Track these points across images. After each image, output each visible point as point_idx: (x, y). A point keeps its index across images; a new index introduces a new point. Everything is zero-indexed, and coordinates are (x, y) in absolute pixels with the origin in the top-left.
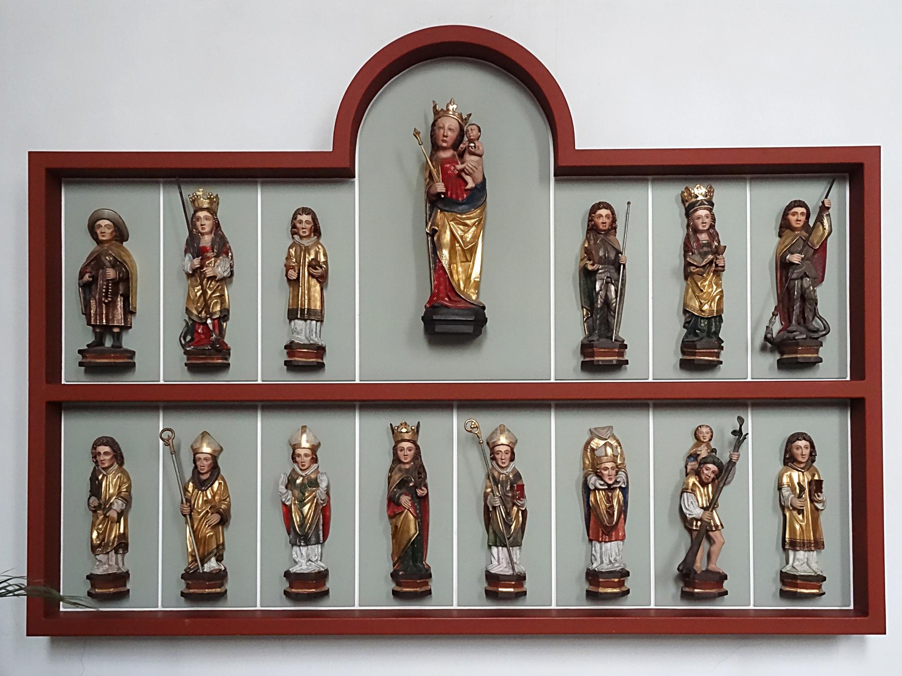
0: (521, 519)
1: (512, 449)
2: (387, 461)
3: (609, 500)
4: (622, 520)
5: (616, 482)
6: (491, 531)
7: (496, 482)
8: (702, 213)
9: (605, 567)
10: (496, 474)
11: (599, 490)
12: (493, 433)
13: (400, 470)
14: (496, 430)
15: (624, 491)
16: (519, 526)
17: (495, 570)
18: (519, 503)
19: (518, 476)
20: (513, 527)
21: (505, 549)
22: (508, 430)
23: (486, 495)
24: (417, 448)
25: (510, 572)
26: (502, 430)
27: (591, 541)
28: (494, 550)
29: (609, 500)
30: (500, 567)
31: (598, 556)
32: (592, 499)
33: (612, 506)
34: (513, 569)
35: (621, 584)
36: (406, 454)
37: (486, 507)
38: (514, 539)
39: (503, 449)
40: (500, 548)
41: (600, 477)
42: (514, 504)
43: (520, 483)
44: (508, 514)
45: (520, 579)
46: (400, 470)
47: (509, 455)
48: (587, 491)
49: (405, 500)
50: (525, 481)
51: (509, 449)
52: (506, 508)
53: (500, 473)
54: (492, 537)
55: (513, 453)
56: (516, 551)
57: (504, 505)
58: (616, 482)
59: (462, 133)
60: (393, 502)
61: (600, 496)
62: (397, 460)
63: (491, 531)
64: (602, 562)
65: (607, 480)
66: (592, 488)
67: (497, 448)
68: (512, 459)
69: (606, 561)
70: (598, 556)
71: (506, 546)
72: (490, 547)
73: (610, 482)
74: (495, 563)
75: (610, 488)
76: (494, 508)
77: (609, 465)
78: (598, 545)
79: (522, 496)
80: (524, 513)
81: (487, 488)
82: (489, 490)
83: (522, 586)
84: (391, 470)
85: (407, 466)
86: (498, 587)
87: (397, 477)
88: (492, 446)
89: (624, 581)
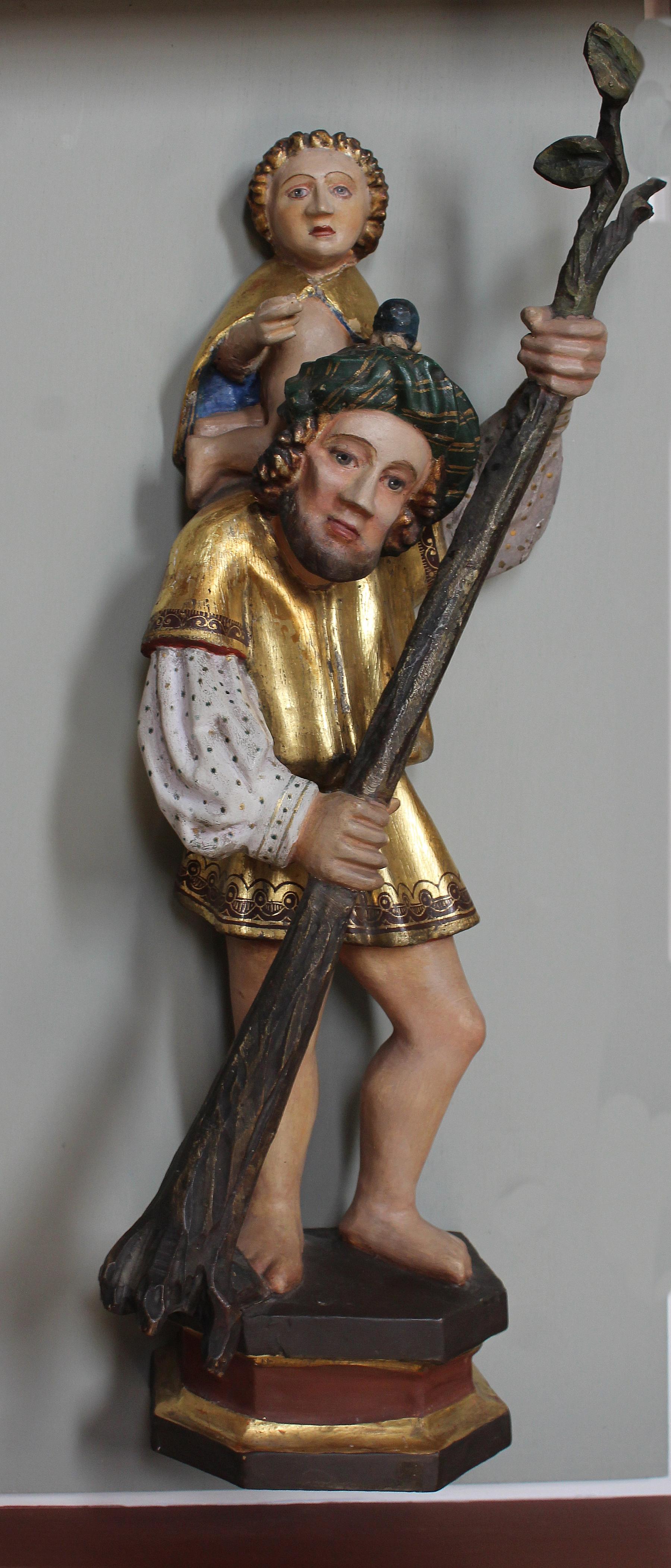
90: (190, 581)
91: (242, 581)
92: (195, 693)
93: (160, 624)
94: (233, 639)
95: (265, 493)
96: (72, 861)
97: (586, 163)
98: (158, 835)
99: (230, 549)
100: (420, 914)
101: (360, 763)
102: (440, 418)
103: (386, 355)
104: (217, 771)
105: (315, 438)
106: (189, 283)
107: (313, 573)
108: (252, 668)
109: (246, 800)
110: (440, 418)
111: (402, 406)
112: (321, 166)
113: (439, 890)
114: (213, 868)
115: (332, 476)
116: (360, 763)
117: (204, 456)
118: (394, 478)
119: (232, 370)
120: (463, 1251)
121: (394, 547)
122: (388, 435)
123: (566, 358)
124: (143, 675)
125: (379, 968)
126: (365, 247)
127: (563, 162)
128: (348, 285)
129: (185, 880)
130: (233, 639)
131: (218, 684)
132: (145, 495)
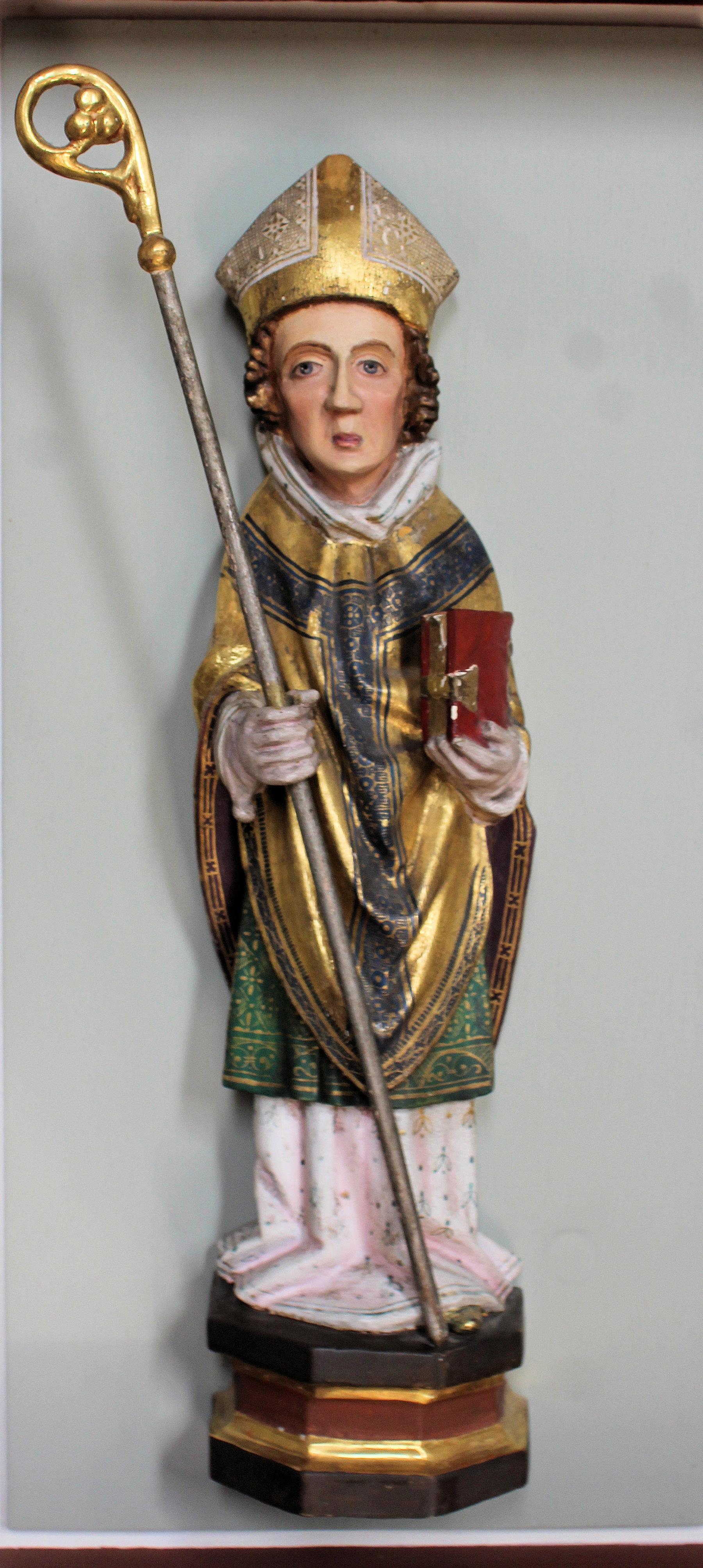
0: (484, 887)
1: (416, 342)
6: (248, 977)
7: (285, 589)
10: (290, 538)
12: (271, 214)
14: (295, 191)
16: (475, 938)
17: (279, 1289)
18: (469, 757)
19: (459, 553)
20: (420, 953)
21: (359, 1125)
22: (382, 195)
23: (210, 696)
25: (399, 1316)
26: (338, 194)
28: (278, 1123)
30: (318, 1270)
34: (417, 1280)
37: (210, 788)
38: (434, 1040)
39: (344, 331)
40: (322, 1115)
42: (429, 771)
43: (475, 602)
44: (381, 843)
45: (485, 1349)
47: (397, 374)
50: (514, 586)
51: (388, 332)
52: (363, 800)
53: (317, 527)
54: (258, 1023)
55: (422, 376)
56: (444, 1148)
57: (350, 775)
59: (277, 743)
63: (248, 977)
67: (298, 328)
68: (415, 422)
71: (358, 1098)
72: (245, 1100)
74: (279, 1224)
76: (275, 798)
79: (495, 703)
80: (510, 843)
81: (217, 639)
82: (239, 654)
83: (492, 1407)
86: (298, 1423)
88: (257, 317)
89: (243, 824)
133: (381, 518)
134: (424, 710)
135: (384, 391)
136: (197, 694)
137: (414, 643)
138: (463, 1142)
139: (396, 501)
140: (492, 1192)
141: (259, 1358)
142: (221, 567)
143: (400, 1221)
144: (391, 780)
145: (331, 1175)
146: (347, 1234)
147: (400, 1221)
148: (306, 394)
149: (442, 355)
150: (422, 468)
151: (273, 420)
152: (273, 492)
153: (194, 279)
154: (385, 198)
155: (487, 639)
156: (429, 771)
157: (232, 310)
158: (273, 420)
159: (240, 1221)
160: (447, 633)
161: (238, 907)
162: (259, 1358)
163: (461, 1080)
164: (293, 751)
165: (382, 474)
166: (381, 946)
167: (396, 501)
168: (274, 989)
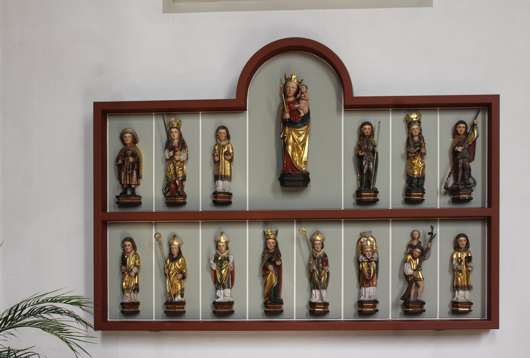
2: (260, 249)
3: (369, 266)
4: (375, 277)
5: (372, 258)
7: (314, 258)
8: (271, 241)
9: (367, 299)
10: (315, 255)
11: (364, 262)
13: (268, 253)
15: (377, 262)
18: (325, 268)
19: (325, 255)
23: (309, 265)
24: (277, 243)
25: (321, 302)
26: (318, 233)
27: (360, 287)
28: (314, 291)
29: (369, 266)
30: (316, 299)
31: (363, 294)
32: (361, 266)
33: (370, 270)
34: (322, 300)
35: (374, 307)
36: (271, 246)
38: (324, 285)
39: (318, 242)
41: (365, 256)
42: (323, 269)
44: (320, 273)
46: (268, 253)
48: (359, 262)
49: (271, 267)
52: (319, 271)
54: (312, 285)
55: (323, 245)
56: (324, 292)
57: (318, 269)
58: (372, 258)
60: (265, 270)
61: (364, 265)
62: (266, 248)
64: (365, 297)
65: (367, 256)
66: (360, 261)
67: (315, 242)
68: (322, 247)
69: (367, 296)
70: (363, 294)
71: (318, 289)
73: (369, 258)
74: (314, 297)
75: (369, 261)
76: (314, 271)
77: (369, 249)
78: (363, 289)
79: (327, 265)
80: (328, 274)
81: (310, 261)
84: (264, 253)
85: (272, 251)
87: (267, 256)
88: (312, 241)
90: (407, 259)
91: (410, 259)
92: (407, 265)
93: (405, 261)
94: (409, 262)
95: (411, 253)
96: (400, 277)
97: (431, 234)
98: (405, 273)
99: (410, 257)
100: (420, 279)
101: (419, 268)
102: (422, 249)
103: (419, 246)
104: (408, 270)
105: (414, 250)
106: (407, 240)
107: (415, 259)
108: (411, 264)
109: (410, 272)
110: (422, 249)
111: (419, 248)
112: (416, 233)
113: (421, 277)
114: (135, 270)
115: (415, 252)
116: (419, 268)
117: (408, 251)
118: (419, 252)
119: (410, 246)
120: (307, 107)
121: (419, 257)
122: (418, 250)
123: (429, 246)
124: (404, 265)
125: (418, 282)
126: (419, 237)
127: (429, 233)
128: (418, 240)
129: (407, 277)
130: (409, 262)
131: (408, 265)
132: (405, 253)
133: (320, 254)
134: (323, 265)
135: (320, 246)
136: (309, 309)
137: (322, 261)
138: (325, 292)
139: (321, 253)
140: (326, 295)
141: (312, 305)
142: (310, 257)
143: (321, 296)
144: (320, 270)
145: (317, 294)
146: (318, 298)
147: (321, 296)
148: (316, 246)
149: (324, 243)
150: (323, 250)
151: (313, 248)
152: (313, 252)
153: (309, 237)
154: (131, 159)
155: (327, 261)
156: (323, 269)
157: (311, 240)
158: (313, 248)
159: (311, 297)
160: (324, 260)
161: (311, 278)
162: (312, 305)
163: (325, 288)
164: (315, 268)
165: (320, 251)
166: (320, 279)
167: (321, 253)
168: (314, 283)
